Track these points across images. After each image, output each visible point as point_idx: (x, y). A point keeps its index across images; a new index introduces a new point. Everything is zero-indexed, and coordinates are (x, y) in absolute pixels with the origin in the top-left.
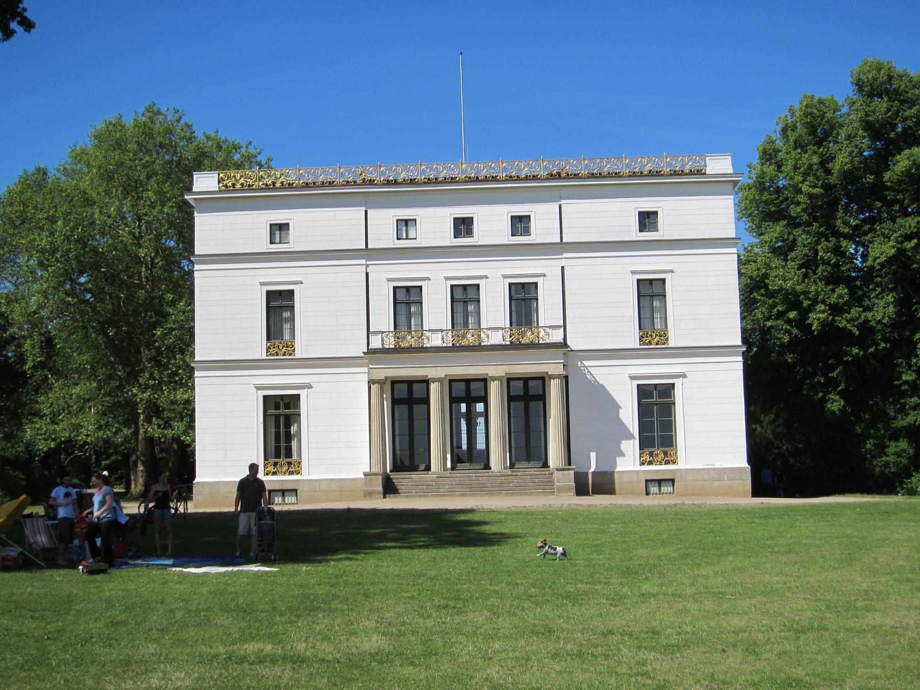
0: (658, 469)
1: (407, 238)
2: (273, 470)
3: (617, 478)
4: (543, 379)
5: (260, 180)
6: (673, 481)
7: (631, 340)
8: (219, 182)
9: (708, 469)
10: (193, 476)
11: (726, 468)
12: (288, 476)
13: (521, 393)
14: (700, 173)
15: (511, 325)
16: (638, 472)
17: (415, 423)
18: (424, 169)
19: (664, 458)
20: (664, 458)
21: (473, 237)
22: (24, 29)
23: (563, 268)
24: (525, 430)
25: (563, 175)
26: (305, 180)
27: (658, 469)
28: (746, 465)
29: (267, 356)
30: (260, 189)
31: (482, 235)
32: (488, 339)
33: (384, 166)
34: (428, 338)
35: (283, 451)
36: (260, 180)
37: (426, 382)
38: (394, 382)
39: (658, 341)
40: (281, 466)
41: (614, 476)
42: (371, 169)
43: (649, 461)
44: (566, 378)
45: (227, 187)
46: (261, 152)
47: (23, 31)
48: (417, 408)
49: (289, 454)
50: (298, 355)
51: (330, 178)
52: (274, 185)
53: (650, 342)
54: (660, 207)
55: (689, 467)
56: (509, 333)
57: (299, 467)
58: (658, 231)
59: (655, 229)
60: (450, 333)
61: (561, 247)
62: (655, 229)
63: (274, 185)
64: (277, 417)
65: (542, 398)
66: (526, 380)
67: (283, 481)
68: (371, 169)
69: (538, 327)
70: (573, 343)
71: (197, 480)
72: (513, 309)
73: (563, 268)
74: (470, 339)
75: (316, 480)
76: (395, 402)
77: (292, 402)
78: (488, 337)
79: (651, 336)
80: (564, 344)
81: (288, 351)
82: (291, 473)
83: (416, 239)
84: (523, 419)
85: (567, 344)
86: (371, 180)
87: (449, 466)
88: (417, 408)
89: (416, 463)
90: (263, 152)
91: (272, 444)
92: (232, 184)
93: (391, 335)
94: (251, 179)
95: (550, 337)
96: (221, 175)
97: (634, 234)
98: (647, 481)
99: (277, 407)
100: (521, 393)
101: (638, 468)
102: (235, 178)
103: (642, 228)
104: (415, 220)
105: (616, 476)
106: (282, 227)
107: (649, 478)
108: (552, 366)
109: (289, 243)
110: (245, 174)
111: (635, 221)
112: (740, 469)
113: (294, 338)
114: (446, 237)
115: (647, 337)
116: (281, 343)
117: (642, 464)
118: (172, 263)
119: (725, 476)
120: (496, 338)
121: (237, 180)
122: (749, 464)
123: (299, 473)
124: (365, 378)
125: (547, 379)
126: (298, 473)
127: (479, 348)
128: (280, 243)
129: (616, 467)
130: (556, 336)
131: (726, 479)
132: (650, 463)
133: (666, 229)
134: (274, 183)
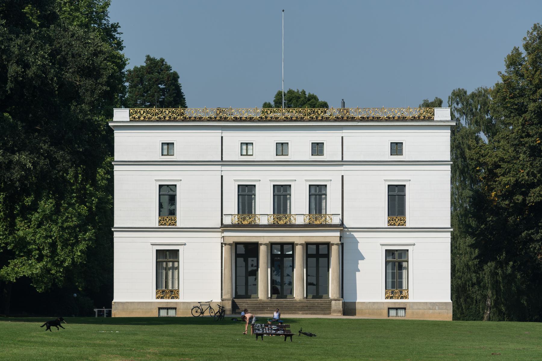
1: (247, 155)
2: (391, 296)
3: (358, 307)
4: (328, 245)
5: (155, 115)
6: (175, 309)
8: (130, 116)
11: (437, 302)
12: (167, 300)
13: (315, 253)
14: (430, 119)
15: (274, 213)
16: (383, 303)
17: (320, 269)
18: (386, 111)
19: (400, 295)
20: (400, 295)
21: (323, 155)
23: (343, 176)
24: (316, 275)
25: (396, 118)
26: (235, 116)
28: (450, 301)
29: (159, 225)
31: (293, 155)
32: (259, 221)
33: (234, 109)
34: (259, 219)
36: (155, 115)
37: (292, 245)
38: (237, 244)
39: (170, 223)
40: (396, 293)
41: (355, 304)
42: (200, 110)
43: (391, 297)
44: (342, 244)
45: (135, 118)
48: (322, 260)
51: (200, 116)
52: (419, 118)
53: (165, 223)
54: (175, 141)
56: (308, 217)
57: (177, 294)
58: (402, 155)
59: (401, 154)
60: (237, 216)
61: (342, 162)
62: (401, 154)
63: (419, 118)
64: (394, 263)
65: (327, 256)
66: (318, 244)
67: (168, 302)
68: (200, 110)
69: (255, 215)
70: (347, 224)
71: (114, 301)
72: (240, 201)
73: (343, 176)
75: (188, 303)
76: (237, 256)
77: (175, 253)
78: (295, 219)
79: (166, 220)
80: (342, 224)
81: (172, 223)
82: (173, 298)
83: (252, 155)
84: (315, 269)
85: (343, 224)
86: (352, 117)
87: (269, 296)
88: (322, 260)
89: (249, 294)
91: (390, 280)
92: (138, 117)
94: (150, 114)
95: (260, 221)
96: (131, 111)
98: (389, 309)
100: (315, 253)
101: (155, 300)
102: (140, 113)
104: (288, 143)
105: (357, 304)
106: (170, 145)
107: (390, 307)
108: (333, 236)
109: (288, 155)
110: (273, 110)
111: (309, 149)
112: (446, 303)
114: (307, 155)
115: (163, 220)
116: (168, 218)
117: (387, 298)
119: (437, 307)
120: (300, 221)
121: (319, 114)
122: (452, 300)
123: (178, 298)
124: (220, 241)
125: (295, 245)
126: (177, 298)
128: (168, 155)
129: (356, 299)
130: (336, 220)
131: (437, 309)
132: (391, 298)
133: (179, 155)
134: (165, 117)
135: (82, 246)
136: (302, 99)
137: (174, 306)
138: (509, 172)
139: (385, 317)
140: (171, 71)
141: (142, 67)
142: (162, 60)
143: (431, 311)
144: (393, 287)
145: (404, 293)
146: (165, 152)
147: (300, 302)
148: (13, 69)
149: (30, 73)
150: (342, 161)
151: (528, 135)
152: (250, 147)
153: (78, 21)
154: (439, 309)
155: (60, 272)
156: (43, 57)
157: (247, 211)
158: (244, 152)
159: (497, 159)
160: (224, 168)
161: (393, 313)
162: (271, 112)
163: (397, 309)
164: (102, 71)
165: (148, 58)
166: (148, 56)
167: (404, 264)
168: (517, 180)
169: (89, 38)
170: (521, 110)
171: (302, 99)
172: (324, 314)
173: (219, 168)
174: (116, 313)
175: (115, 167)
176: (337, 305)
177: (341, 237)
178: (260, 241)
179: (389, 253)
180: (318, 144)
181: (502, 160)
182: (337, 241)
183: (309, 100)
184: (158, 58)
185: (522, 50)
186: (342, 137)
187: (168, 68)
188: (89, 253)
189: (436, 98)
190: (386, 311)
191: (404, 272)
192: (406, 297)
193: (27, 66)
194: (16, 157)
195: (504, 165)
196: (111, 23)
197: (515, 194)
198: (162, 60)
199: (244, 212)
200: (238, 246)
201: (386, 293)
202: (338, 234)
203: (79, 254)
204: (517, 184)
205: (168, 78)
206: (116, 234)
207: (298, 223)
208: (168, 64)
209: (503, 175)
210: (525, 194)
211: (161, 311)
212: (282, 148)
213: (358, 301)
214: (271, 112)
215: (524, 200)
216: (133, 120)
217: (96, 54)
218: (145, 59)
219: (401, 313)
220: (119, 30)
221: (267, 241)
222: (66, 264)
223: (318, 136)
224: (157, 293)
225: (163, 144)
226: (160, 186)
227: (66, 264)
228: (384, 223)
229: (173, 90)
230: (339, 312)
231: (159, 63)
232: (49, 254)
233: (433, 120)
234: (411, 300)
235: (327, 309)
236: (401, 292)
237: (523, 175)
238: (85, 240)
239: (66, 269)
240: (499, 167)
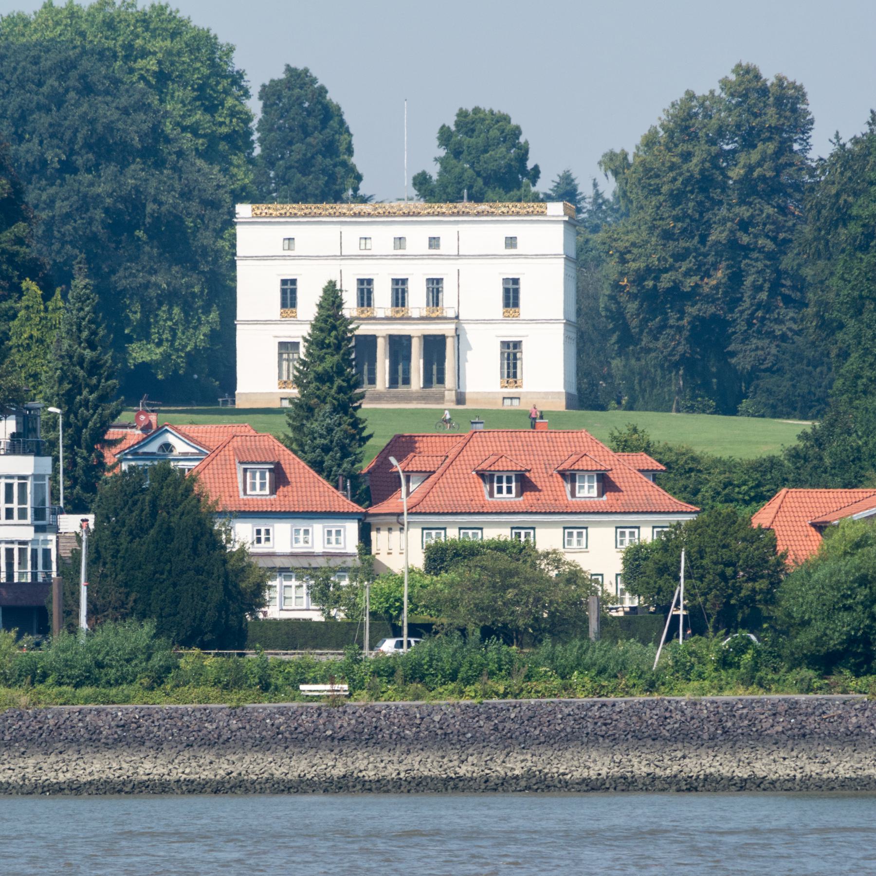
0: (511, 391)
3: (467, 396)
10: (235, 389)
14: (542, 213)
16: (498, 393)
22: (708, 104)
25: (362, 214)
27: (511, 391)
30: (327, 216)
37: (409, 338)
44: (458, 336)
47: (482, 107)
49: (515, 376)
61: (459, 256)
71: (237, 392)
77: (517, 345)
80: (457, 317)
97: (501, 249)
98: (504, 398)
99: (509, 348)
103: (430, 246)
106: (290, 240)
108: (447, 329)
112: (559, 393)
114: (389, 249)
117: (502, 387)
127: (375, 318)
130: (451, 314)
135: (205, 329)
136: (487, 122)
138: (639, 257)
139: (500, 407)
140: (316, 86)
141: (280, 81)
142: (306, 71)
144: (508, 376)
145: (518, 384)
146: (286, 247)
147: (417, 392)
148: (150, 207)
149: (164, 209)
150: (458, 255)
151: (661, 219)
153: (199, 73)
155: (182, 357)
156: (174, 197)
157: (365, 303)
158: (363, 247)
159: (627, 244)
161: (508, 402)
163: (511, 398)
164: (223, 203)
165: (289, 69)
166: (288, 66)
167: (518, 355)
168: (647, 266)
169: (212, 174)
170: (657, 191)
171: (487, 122)
173: (338, 262)
174: (240, 404)
176: (450, 395)
177: (456, 329)
179: (505, 344)
180: (434, 238)
181: (634, 244)
182: (453, 333)
183: (498, 122)
184: (300, 67)
185: (659, 129)
187: (314, 81)
188: (213, 336)
189: (600, 163)
191: (519, 363)
192: (521, 387)
193: (161, 204)
194: (153, 279)
195: (635, 251)
196: (236, 69)
197: (645, 280)
198: (306, 71)
199: (362, 305)
202: (453, 326)
203: (202, 337)
204: (648, 269)
205: (313, 96)
206: (238, 327)
207: (414, 316)
208: (314, 75)
209: (634, 261)
210: (657, 279)
211: (505, 401)
213: (468, 390)
215: (655, 286)
217: (219, 187)
218: (283, 69)
219: (516, 402)
220: (246, 78)
221: (384, 333)
222: (188, 349)
223: (434, 231)
224: (279, 384)
225: (285, 239)
227: (188, 349)
229: (319, 110)
230: (452, 401)
231: (303, 75)
232: (170, 338)
233: (546, 215)
235: (441, 398)
236: (516, 382)
237: (654, 260)
238: (208, 322)
239: (188, 354)
240: (629, 252)
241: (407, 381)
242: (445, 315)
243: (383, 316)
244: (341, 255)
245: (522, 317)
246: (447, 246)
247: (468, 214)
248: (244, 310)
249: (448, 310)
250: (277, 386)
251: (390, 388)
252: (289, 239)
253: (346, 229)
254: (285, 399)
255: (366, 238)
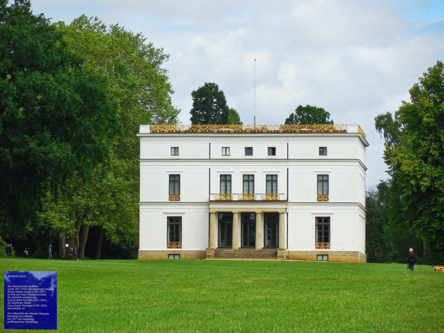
1: (226, 155)
7: (314, 198)
9: (342, 251)
16: (314, 252)
31: (256, 154)
35: (174, 239)
37: (255, 214)
46: (145, 40)
50: (329, 202)
55: (334, 250)
61: (288, 159)
71: (140, 250)
74: (228, 198)
82: (178, 248)
90: (146, 39)
93: (218, 195)
97: (317, 156)
98: (317, 255)
106: (175, 148)
107: (318, 254)
113: (180, 194)
114: (242, 154)
117: (168, 248)
118: (381, 326)
126: (181, 248)
133: (182, 155)
137: (179, 253)
143: (345, 257)
146: (173, 153)
152: (228, 149)
154: (350, 255)
158: (224, 154)
160: (290, 163)
162: (225, 127)
163: (322, 255)
172: (230, 261)
175: (141, 163)
178: (233, 211)
179: (319, 219)
186: (288, 144)
190: (316, 256)
200: (220, 214)
201: (316, 246)
211: (318, 256)
212: (249, 151)
214: (225, 127)
216: (153, 132)
221: (260, 211)
226: (221, 175)
228: (167, 200)
233: (346, 133)
234: (331, 250)
241: (253, 244)
242: (278, 199)
243: (237, 199)
244: (288, 159)
245: (330, 201)
246: (280, 153)
247: (212, 132)
248: (144, 196)
249: (257, 195)
250: (314, 247)
251: (242, 247)
252: (175, 148)
253: (212, 140)
254: (319, 255)
255: (226, 148)
